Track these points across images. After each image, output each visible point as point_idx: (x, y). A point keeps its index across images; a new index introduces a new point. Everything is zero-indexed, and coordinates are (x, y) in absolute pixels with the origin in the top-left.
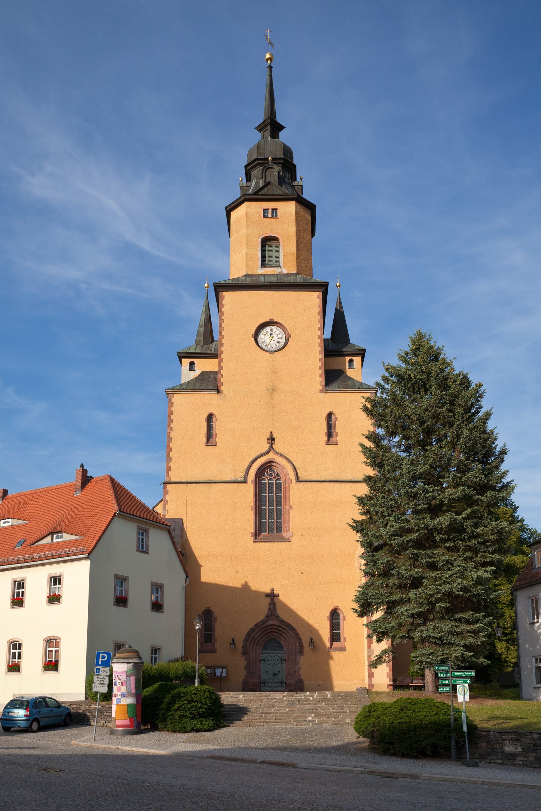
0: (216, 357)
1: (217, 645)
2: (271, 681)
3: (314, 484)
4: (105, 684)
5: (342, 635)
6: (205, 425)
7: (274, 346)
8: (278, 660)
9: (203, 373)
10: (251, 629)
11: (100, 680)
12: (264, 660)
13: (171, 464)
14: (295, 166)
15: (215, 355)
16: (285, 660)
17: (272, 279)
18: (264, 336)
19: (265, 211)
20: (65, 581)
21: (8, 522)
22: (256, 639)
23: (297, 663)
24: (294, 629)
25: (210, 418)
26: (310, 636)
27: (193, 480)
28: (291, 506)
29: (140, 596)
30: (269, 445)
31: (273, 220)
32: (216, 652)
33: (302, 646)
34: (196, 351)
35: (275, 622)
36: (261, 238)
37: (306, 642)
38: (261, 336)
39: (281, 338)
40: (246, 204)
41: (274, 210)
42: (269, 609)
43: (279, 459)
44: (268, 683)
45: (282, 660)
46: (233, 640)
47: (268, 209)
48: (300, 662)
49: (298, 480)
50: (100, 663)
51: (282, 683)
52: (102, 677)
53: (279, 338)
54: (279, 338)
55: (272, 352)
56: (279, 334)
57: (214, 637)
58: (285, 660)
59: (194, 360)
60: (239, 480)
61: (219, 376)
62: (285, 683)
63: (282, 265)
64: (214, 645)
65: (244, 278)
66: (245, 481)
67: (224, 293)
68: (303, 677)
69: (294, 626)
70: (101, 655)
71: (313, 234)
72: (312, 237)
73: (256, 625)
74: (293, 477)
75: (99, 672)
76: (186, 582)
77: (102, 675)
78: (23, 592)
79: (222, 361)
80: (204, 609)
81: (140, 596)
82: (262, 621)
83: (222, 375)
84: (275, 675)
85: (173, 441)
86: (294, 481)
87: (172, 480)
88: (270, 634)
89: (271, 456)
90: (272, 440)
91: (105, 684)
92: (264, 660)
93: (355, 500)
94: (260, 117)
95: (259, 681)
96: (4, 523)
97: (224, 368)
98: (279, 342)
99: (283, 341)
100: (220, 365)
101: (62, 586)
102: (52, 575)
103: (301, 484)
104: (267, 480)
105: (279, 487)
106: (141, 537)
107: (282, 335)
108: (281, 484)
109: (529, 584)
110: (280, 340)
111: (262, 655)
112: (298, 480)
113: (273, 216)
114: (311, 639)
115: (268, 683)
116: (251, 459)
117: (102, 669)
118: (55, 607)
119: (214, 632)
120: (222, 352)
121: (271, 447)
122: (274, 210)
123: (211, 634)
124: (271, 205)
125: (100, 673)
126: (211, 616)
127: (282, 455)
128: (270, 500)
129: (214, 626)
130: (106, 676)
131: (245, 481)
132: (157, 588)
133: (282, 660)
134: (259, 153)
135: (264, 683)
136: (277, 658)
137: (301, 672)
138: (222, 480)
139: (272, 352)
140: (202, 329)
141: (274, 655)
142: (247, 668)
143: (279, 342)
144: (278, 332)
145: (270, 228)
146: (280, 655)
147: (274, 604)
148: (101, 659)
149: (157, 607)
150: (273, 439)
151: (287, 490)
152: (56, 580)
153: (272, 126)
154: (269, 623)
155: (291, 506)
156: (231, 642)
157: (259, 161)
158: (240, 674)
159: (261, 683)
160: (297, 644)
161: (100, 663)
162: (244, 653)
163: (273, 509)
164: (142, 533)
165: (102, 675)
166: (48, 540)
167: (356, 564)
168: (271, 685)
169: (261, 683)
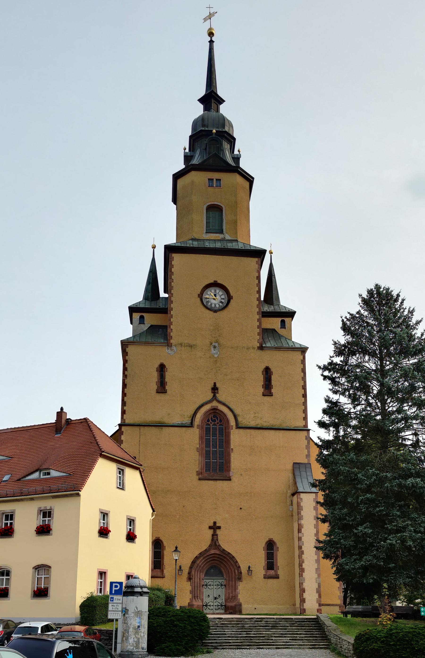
1: (165, 571)
2: (212, 604)
3: (252, 431)
4: (119, 611)
5: (275, 564)
6: (155, 375)
7: (217, 306)
8: (218, 585)
9: (151, 326)
10: (196, 557)
11: (114, 607)
12: (206, 585)
13: (125, 408)
14: (234, 139)
16: (225, 585)
17: (231, 244)
18: (210, 294)
19: (211, 180)
20: (56, 514)
22: (200, 567)
23: (236, 588)
24: (233, 557)
25: (162, 368)
26: (249, 565)
28: (232, 449)
29: (118, 529)
30: (213, 394)
31: (217, 190)
32: (164, 577)
33: (241, 573)
34: (146, 306)
36: (223, 207)
37: (244, 570)
38: (205, 296)
39: (223, 299)
40: (193, 173)
41: (219, 180)
42: (212, 540)
43: (222, 408)
44: (210, 606)
45: (222, 585)
47: (213, 179)
48: (239, 587)
49: (238, 427)
50: (113, 592)
51: (222, 606)
52: (116, 605)
53: (222, 299)
54: (222, 299)
56: (222, 295)
57: (163, 564)
58: (225, 585)
60: (186, 425)
62: (225, 606)
63: (224, 231)
64: (163, 571)
66: (191, 425)
67: (174, 255)
68: (241, 601)
69: (233, 555)
70: (114, 584)
73: (200, 554)
74: (232, 422)
75: (113, 601)
76: (152, 516)
78: (11, 524)
79: (259, 327)
81: (118, 529)
82: (206, 550)
83: (172, 329)
84: (215, 598)
85: (127, 387)
86: (234, 427)
87: (127, 422)
88: (213, 562)
89: (215, 404)
90: (215, 389)
91: (119, 611)
92: (206, 585)
93: (204, 544)
94: (202, 92)
95: (202, 604)
97: (173, 324)
98: (221, 302)
99: (225, 301)
100: (260, 323)
102: (42, 508)
103: (241, 431)
104: (211, 425)
106: (119, 475)
108: (223, 429)
110: (223, 301)
111: (205, 580)
114: (249, 567)
115: (210, 606)
116: (197, 406)
117: (115, 597)
118: (44, 538)
119: (163, 558)
120: (172, 309)
121: (214, 398)
122: (219, 180)
123: (160, 561)
124: (215, 175)
125: (114, 601)
126: (160, 545)
128: (213, 443)
129: (163, 554)
132: (131, 521)
133: (222, 585)
135: (206, 606)
137: (240, 596)
139: (215, 311)
140: (150, 286)
141: (215, 581)
142: (191, 592)
143: (221, 302)
145: (215, 197)
146: (220, 581)
147: (217, 535)
148: (114, 589)
149: (131, 537)
150: (217, 389)
151: (228, 435)
152: (47, 514)
153: (211, 99)
154: (212, 552)
155: (232, 449)
157: (203, 133)
160: (236, 571)
161: (113, 592)
162: (189, 579)
164: (121, 472)
166: (35, 476)
167: (288, 501)
168: (212, 607)
169: (203, 606)
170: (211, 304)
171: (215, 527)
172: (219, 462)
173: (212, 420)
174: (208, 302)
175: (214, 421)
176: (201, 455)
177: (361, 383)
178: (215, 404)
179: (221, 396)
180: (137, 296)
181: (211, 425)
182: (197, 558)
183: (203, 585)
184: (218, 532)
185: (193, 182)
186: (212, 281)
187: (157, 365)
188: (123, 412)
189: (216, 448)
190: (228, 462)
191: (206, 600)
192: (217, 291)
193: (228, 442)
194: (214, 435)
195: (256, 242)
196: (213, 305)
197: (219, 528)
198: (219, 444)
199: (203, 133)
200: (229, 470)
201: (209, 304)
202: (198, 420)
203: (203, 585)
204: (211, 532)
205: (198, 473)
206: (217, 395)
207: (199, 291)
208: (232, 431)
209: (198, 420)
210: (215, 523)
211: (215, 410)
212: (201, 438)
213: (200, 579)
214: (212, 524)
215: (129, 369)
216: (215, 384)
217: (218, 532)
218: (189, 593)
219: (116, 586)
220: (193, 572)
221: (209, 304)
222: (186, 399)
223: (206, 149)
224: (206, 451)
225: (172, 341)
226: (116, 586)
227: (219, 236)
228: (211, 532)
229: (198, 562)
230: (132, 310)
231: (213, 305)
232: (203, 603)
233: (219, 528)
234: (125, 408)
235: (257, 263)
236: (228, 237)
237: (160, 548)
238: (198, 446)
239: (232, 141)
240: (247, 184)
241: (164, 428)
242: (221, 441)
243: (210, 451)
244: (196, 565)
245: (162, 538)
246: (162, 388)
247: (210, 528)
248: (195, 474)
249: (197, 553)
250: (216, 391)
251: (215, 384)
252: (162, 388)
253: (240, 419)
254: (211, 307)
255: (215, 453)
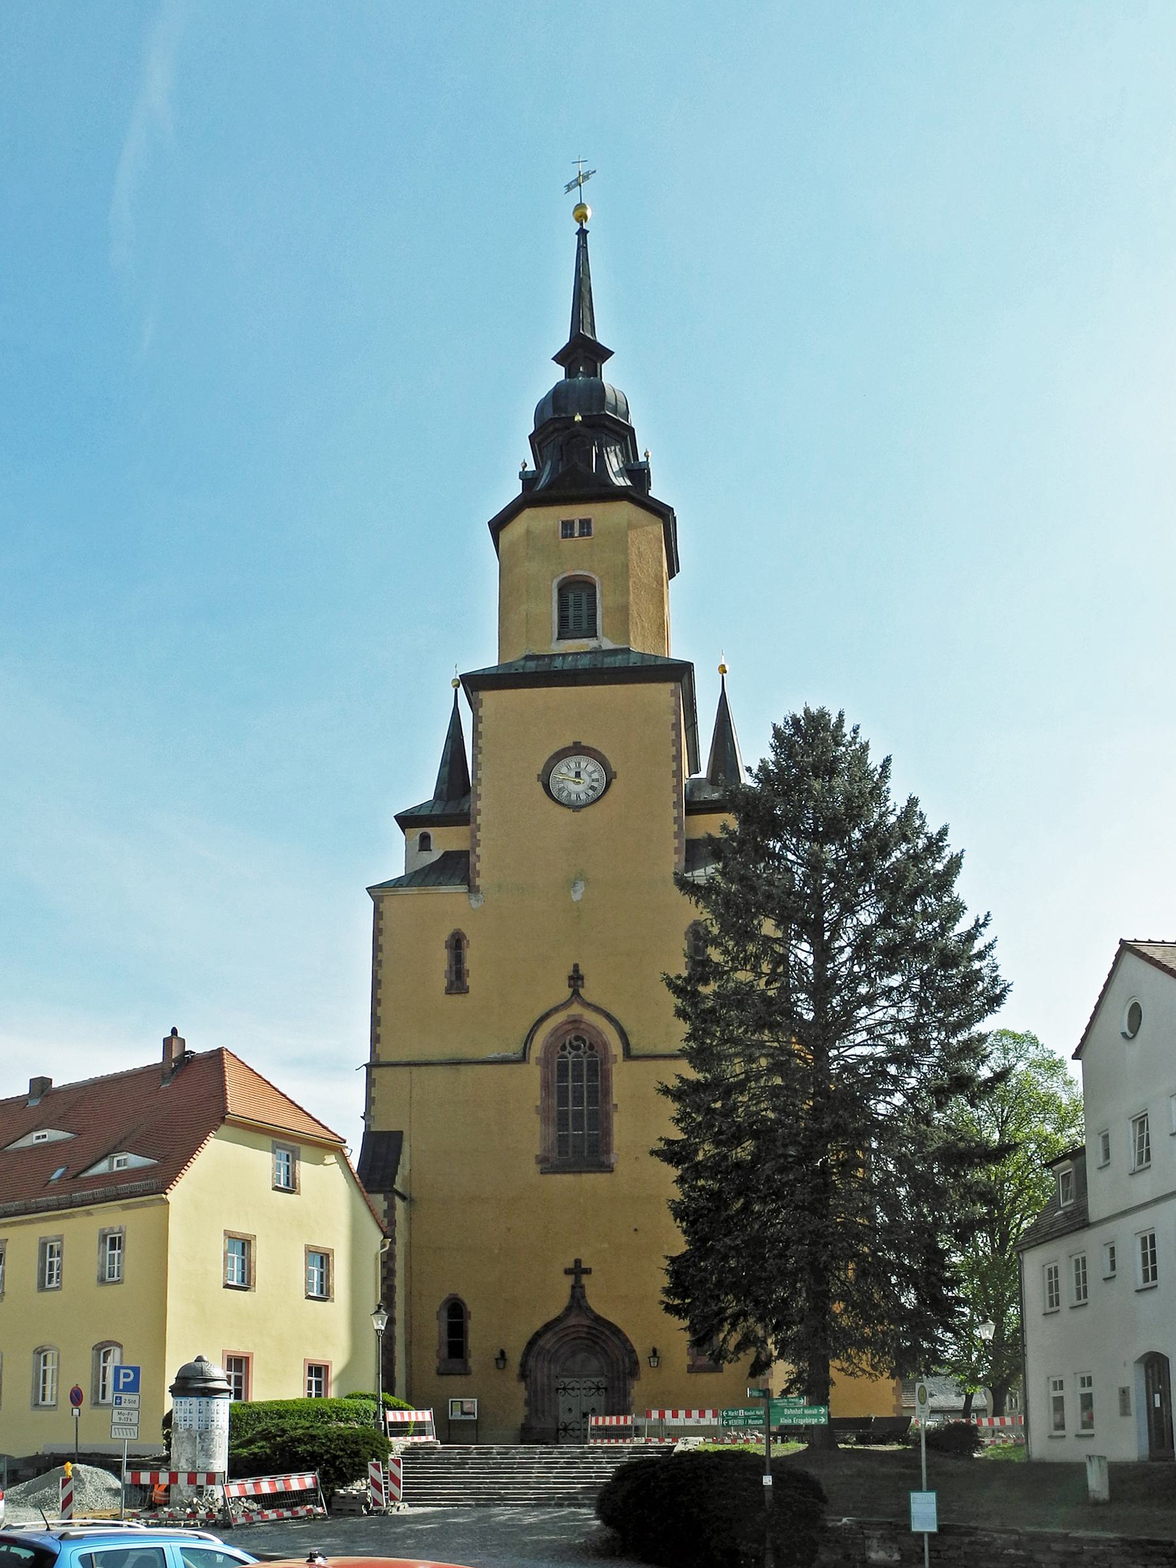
0: (466, 822)
2: (577, 1426)
7: (583, 796)
8: (590, 1389)
9: (447, 854)
12: (564, 1389)
13: (379, 1030)
14: (631, 431)
15: (463, 819)
16: (606, 1389)
18: (564, 770)
19: (567, 526)
21: (38, 1138)
24: (619, 1331)
25: (457, 943)
27: (423, 1059)
30: (571, 990)
33: (637, 1363)
35: (586, 1322)
38: (555, 777)
40: (528, 513)
41: (586, 524)
42: (573, 1296)
44: (573, 1429)
45: (598, 1389)
46: (503, 1353)
49: (628, 1055)
52: (126, 1412)
55: (577, 808)
58: (606, 1389)
59: (430, 831)
61: (472, 859)
64: (466, 1363)
65: (522, 663)
66: (523, 1059)
70: (122, 1371)
71: (673, 570)
72: (671, 575)
74: (616, 1048)
76: (383, 1246)
77: (126, 1409)
80: (445, 1296)
82: (558, 1320)
83: (478, 857)
87: (383, 1059)
90: (576, 979)
92: (564, 1389)
96: (44, 1136)
98: (592, 788)
101: (123, 1251)
103: (635, 1064)
105: (593, 1068)
107: (599, 775)
109: (111, 1190)
110: (595, 784)
112: (628, 1055)
113: (582, 535)
119: (466, 1338)
120: (479, 812)
121: (576, 993)
122: (586, 524)
124: (576, 512)
125: (123, 1405)
127: (597, 1009)
130: (1023, 1443)
131: (523, 1059)
133: (598, 1389)
134: (556, 409)
135: (565, 1429)
136: (589, 1384)
138: (482, 1057)
139: (577, 808)
142: (527, 1403)
143: (592, 788)
144: (590, 768)
145: (577, 559)
146: (595, 1380)
147: (582, 1287)
148: (122, 1380)
150: (581, 978)
151: (606, 1076)
153: (583, 353)
154: (572, 1321)
156: (498, 1355)
158: (519, 1415)
159: (558, 1430)
160: (627, 1360)
162: (523, 1375)
163: (567, 1112)
165: (126, 1409)
168: (578, 1433)
169: (558, 1430)
170: (569, 794)
171: (578, 1271)
172: (589, 1135)
173: (572, 1046)
174: (561, 790)
175: (578, 1048)
176: (545, 1120)
177: (779, 975)
178: (576, 1009)
179: (589, 992)
180: (422, 790)
181: (570, 1057)
182: (538, 1335)
183: (558, 1389)
184: (585, 1279)
185: (528, 532)
186: (569, 743)
187: (445, 936)
188: (375, 1039)
189: (582, 1104)
190: (607, 1133)
191: (565, 1418)
192: (583, 765)
193: (607, 1092)
194: (578, 1078)
195: (677, 652)
196: (574, 797)
197: (588, 1271)
198: (589, 1097)
199: (557, 425)
200: (608, 1151)
201: (565, 794)
202: (537, 1049)
203: (558, 1389)
204: (570, 1280)
205: (542, 1160)
206: (581, 991)
207: (539, 767)
208: (615, 1069)
209: (537, 1049)
210: (578, 1262)
211: (575, 1022)
212: (546, 1085)
213: (549, 1376)
214: (571, 1265)
215: (386, 948)
216: (576, 966)
217: (585, 1279)
218: (522, 1404)
219: (126, 1376)
220: (531, 1362)
221: (565, 794)
222: (513, 1002)
223: (562, 459)
224: (560, 1112)
225: (478, 881)
226: (126, 1376)
227: (588, 644)
228: (570, 1280)
229: (541, 1342)
230: (406, 821)
231: (574, 797)
232: (557, 1423)
233: (588, 1271)
234: (379, 1030)
235: (674, 693)
236: (607, 644)
237: (461, 1317)
238: (539, 1103)
239: (624, 435)
240: (658, 528)
241: (462, 1068)
242: (593, 1091)
243: (567, 1112)
244: (536, 1348)
245: (463, 1296)
246: (457, 982)
247: (568, 1272)
248: (534, 1161)
249: (538, 1325)
250: (580, 983)
251: (576, 966)
252: (457, 982)
253: (633, 1041)
254: (570, 800)
255: (578, 1115)
